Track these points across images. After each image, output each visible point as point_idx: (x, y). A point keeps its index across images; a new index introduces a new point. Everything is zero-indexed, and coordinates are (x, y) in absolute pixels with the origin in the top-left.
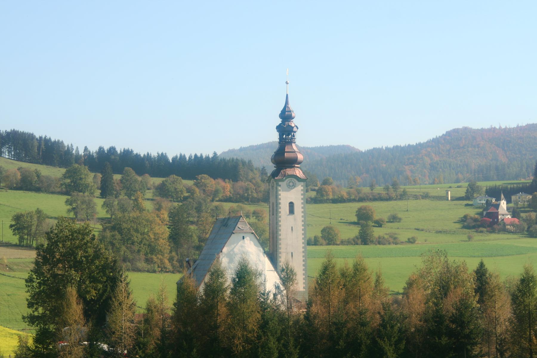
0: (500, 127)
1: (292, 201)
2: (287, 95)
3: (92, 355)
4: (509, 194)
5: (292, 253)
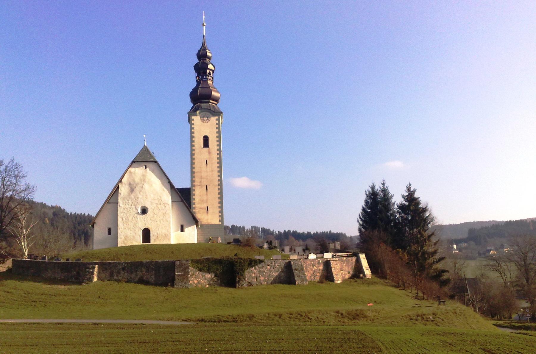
0: (453, 224)
1: (206, 135)
2: (202, 56)
3: (1, 306)
4: (457, 242)
5: (207, 186)
